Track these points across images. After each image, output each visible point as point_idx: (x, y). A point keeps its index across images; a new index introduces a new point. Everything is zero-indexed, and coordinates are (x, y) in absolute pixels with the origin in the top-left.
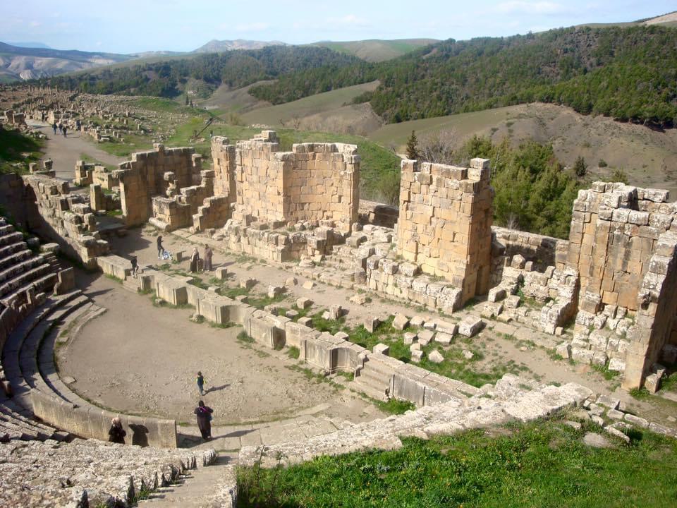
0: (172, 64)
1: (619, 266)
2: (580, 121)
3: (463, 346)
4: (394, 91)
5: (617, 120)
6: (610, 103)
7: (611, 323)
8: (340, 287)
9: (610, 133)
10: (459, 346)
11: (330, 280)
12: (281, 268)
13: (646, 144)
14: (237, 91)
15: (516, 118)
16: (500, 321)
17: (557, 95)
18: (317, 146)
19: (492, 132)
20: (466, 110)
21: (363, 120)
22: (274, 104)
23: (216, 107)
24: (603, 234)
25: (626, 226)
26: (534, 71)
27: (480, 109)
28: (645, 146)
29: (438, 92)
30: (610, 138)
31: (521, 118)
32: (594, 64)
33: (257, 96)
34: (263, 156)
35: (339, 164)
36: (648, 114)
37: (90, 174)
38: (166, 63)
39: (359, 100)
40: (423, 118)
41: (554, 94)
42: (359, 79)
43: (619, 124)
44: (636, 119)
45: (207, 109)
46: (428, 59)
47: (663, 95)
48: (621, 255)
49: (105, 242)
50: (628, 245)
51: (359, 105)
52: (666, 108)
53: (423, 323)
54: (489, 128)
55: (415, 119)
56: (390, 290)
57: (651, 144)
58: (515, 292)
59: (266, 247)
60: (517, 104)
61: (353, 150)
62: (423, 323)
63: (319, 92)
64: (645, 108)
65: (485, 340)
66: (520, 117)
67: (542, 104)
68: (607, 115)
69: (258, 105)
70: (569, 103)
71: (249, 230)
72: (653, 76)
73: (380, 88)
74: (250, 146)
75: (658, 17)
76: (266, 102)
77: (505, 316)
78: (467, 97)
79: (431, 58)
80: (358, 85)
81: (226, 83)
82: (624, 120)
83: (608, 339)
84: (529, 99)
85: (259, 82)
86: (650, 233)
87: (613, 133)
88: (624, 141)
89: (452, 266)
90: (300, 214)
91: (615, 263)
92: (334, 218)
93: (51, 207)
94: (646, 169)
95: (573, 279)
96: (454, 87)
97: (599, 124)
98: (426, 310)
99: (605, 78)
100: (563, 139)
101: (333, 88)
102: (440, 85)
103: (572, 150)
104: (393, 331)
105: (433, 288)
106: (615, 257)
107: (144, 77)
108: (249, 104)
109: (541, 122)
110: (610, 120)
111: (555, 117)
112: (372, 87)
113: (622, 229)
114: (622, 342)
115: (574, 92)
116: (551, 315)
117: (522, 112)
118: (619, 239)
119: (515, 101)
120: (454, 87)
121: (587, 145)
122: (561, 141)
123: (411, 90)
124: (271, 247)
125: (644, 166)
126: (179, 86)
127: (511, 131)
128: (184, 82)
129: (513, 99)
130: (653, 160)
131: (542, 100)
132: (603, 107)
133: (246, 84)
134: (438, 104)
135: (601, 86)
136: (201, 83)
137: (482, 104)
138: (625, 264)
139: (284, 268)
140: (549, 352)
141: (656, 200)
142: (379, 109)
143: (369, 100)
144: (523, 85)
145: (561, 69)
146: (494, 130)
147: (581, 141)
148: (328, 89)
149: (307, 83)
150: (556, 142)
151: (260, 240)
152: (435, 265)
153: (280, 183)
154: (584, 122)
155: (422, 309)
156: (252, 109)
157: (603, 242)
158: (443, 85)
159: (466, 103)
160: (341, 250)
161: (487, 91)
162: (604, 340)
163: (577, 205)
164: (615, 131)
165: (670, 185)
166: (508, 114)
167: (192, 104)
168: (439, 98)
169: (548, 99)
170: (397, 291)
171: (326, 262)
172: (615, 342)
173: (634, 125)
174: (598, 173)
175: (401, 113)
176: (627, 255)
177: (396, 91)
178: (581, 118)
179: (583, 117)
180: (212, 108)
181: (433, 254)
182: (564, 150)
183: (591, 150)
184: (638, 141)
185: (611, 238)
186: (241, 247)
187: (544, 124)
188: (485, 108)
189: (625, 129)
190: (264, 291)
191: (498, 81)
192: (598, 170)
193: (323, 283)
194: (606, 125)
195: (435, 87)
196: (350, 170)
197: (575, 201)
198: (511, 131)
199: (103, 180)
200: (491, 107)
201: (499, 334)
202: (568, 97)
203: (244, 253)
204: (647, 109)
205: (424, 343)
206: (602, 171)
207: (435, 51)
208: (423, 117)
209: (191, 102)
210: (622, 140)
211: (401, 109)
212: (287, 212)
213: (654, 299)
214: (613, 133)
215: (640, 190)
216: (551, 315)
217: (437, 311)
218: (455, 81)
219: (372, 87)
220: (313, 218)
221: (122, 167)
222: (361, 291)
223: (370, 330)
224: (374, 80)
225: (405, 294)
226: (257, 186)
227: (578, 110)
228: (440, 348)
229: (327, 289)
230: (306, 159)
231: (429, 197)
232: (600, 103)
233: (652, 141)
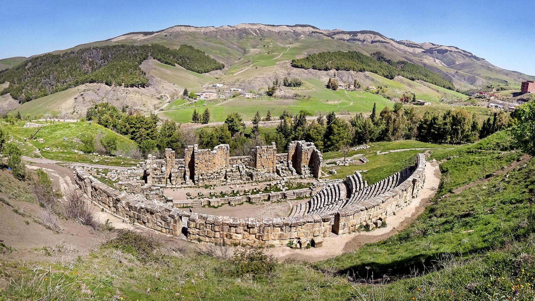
27: (64, 90)
66: (84, 91)
73: (10, 86)
112: (7, 85)
119: (77, 84)
121: (118, 99)
127: (83, 98)
143: (9, 92)
146: (76, 98)
147: (115, 98)
150: (104, 99)
169: (92, 81)
184: (137, 95)
198: (83, 98)
210: (131, 95)
214: (127, 93)
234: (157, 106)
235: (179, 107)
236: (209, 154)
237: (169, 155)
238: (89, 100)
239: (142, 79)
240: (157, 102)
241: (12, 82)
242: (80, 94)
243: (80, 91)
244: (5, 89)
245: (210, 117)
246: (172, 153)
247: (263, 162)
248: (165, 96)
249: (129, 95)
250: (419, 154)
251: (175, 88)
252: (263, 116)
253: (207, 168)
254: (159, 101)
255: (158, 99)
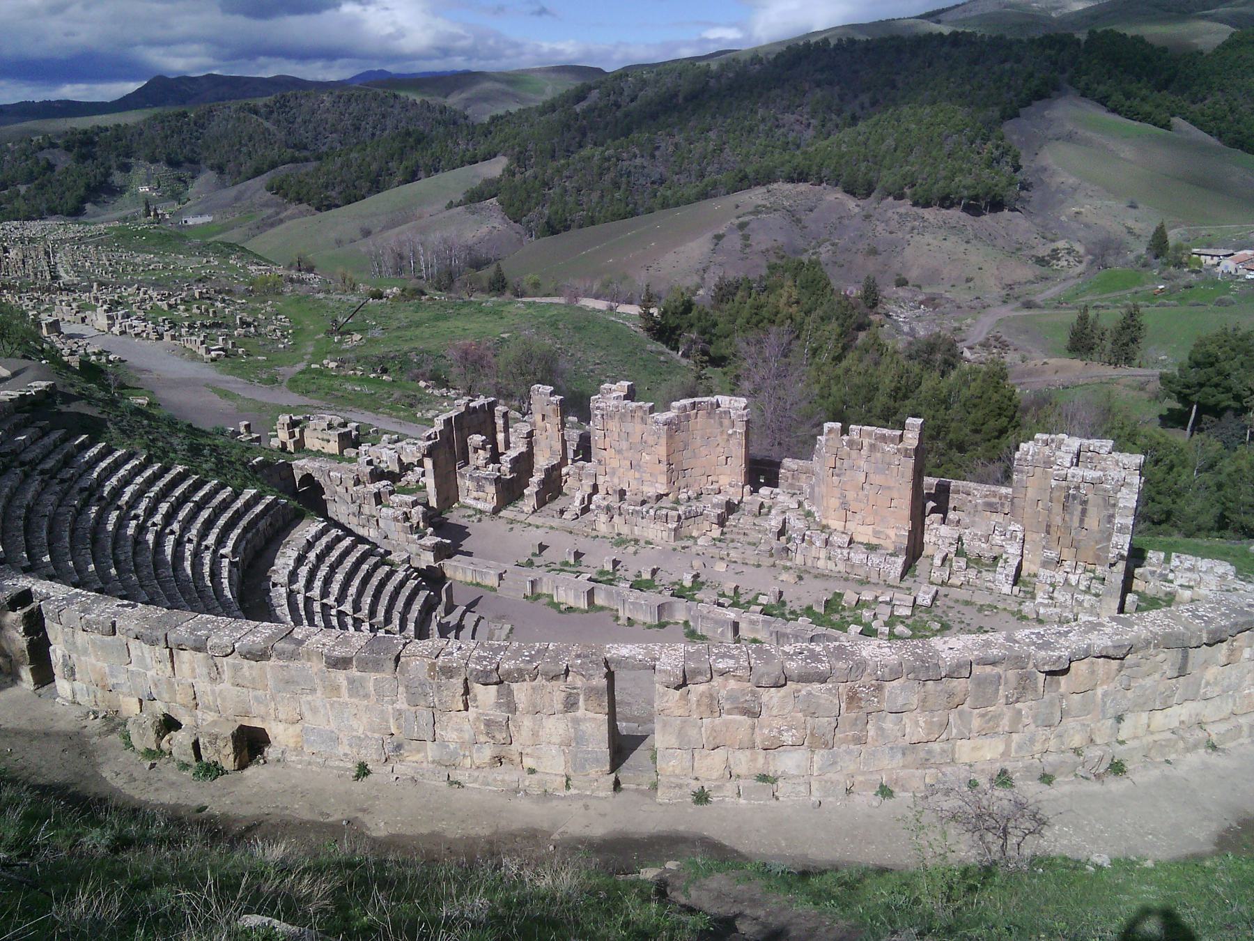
0: (97, 134)
1: (1076, 523)
2: (857, 210)
3: (925, 617)
4: (536, 178)
5: (915, 204)
6: (904, 177)
7: (1073, 579)
8: (759, 566)
9: (908, 229)
10: (920, 617)
11: (744, 559)
12: (674, 550)
13: (967, 242)
14: (241, 187)
15: (751, 213)
16: (952, 586)
17: (815, 168)
18: (700, 403)
19: (716, 241)
20: (665, 205)
21: (490, 232)
22: (319, 209)
23: (207, 218)
24: (1058, 494)
25: (1082, 486)
26: (769, 124)
27: (689, 202)
28: (965, 246)
29: (612, 175)
30: (908, 237)
31: (760, 212)
32: (867, 105)
33: (285, 196)
34: (637, 420)
35: (726, 422)
36: (966, 193)
37: (302, 432)
38: (85, 132)
39: (475, 197)
40: (593, 223)
41: (810, 167)
42: (468, 154)
43: (920, 211)
44: (946, 201)
45: (190, 223)
46: (584, 111)
47: (985, 155)
48: (1077, 513)
49: (449, 541)
50: (1085, 502)
51: (477, 205)
52: (993, 178)
53: (877, 597)
54: (709, 235)
55: (581, 227)
56: (821, 564)
57: (973, 242)
58: (959, 553)
59: (652, 526)
60: (749, 187)
61: (743, 405)
62: (877, 597)
63: (401, 183)
64: (960, 181)
65: (945, 608)
66: (757, 211)
67: (790, 186)
68: (900, 197)
69: (289, 212)
70: (835, 181)
71: (625, 506)
72: (966, 125)
73: (510, 172)
74: (617, 407)
75: (957, 6)
76: (304, 206)
77: (955, 580)
78: (662, 181)
79: (591, 110)
80: (467, 168)
81: (212, 168)
82: (927, 205)
83: (1073, 595)
84: (765, 178)
85: (281, 168)
86: (1105, 490)
87: (913, 229)
88: (931, 241)
89: (892, 533)
90: (682, 482)
91: (1071, 520)
92: (721, 482)
93: (353, 502)
94: (971, 284)
95: (1020, 535)
96: (638, 161)
97: (890, 213)
98: (869, 582)
99: (891, 131)
100: (833, 245)
101: (422, 174)
102: (614, 160)
103: (850, 262)
104: (844, 609)
105: (875, 559)
106: (1072, 514)
107: (43, 163)
108: (270, 211)
109: (793, 216)
110: (905, 206)
111: (816, 207)
112: (495, 168)
113: (1077, 488)
114: (1087, 597)
115: (843, 161)
116: (1007, 575)
117: (760, 202)
118: (1074, 497)
119: (743, 182)
120: (638, 161)
121: (873, 252)
122: (830, 247)
123: (566, 173)
124: (659, 526)
125: (968, 280)
126: (117, 178)
127: (746, 237)
128: (126, 168)
129: (741, 180)
130: (980, 269)
131: (791, 180)
132: (893, 184)
133: (258, 172)
134: (617, 195)
135: (884, 147)
136: (162, 169)
137: (691, 191)
138: (1082, 521)
139: (680, 549)
140: (1013, 614)
141: (1101, 451)
142: (515, 214)
144: (753, 151)
145: (813, 117)
146: (719, 238)
148: (412, 177)
149: (374, 167)
151: (643, 518)
152: (871, 533)
153: (662, 451)
154: (864, 213)
155: (864, 582)
156: (281, 221)
157: (1059, 501)
158: (618, 160)
159: (661, 191)
160: (741, 521)
161: (695, 166)
162: (1068, 597)
163: (1020, 459)
164: (916, 223)
165: (1012, 310)
166: (737, 207)
167: (156, 215)
168: (617, 186)
169: (799, 176)
170: (831, 565)
171: (727, 536)
172: (1081, 597)
173: (944, 211)
174: (895, 296)
175: (553, 217)
176: (1084, 512)
177: (540, 177)
178: (857, 206)
179: (861, 203)
180: (200, 220)
181: (868, 520)
182: (836, 263)
183: (880, 259)
184: (953, 238)
185: (1067, 497)
186: (613, 526)
187: (799, 221)
188: (698, 199)
189: (931, 220)
190: (674, 578)
191: (711, 147)
192: (894, 293)
193: (735, 562)
194: (901, 215)
195: (606, 164)
196: (740, 429)
197: (1017, 455)
198: (746, 237)
199: (328, 441)
200: (704, 195)
201: (957, 601)
202: (835, 170)
203: (619, 534)
204: (963, 183)
205: (886, 618)
206: (901, 292)
207: (595, 94)
208: (593, 222)
209: (155, 210)
210: (928, 238)
211: (554, 208)
212: (671, 482)
213: (1122, 557)
214: (913, 229)
215: (1086, 442)
216: (1007, 575)
217: (882, 582)
218: (637, 152)
219: (495, 168)
220: (696, 485)
221: (429, 438)
222: (786, 568)
223: (822, 610)
224: (495, 156)
225: (841, 567)
226: (629, 454)
227: (850, 191)
228: (902, 622)
229: (744, 569)
230: (688, 418)
231: (862, 463)
232: (887, 178)
233: (976, 237)
234: (1017, 290)
235: (1102, 300)
236: (644, 421)
237: (542, 409)
238: (764, 247)
239: (998, 178)
240: (1024, 272)
241: (521, 159)
242: (737, 222)
243: (740, 211)
244: (489, 182)
245: (1143, 343)
246: (549, 403)
247: (851, 495)
248: (1070, 251)
249: (917, 238)
250: (922, 420)
251: (1130, 223)
252: (628, 317)
253: (637, 475)
254: (1040, 270)
255: (1041, 261)
